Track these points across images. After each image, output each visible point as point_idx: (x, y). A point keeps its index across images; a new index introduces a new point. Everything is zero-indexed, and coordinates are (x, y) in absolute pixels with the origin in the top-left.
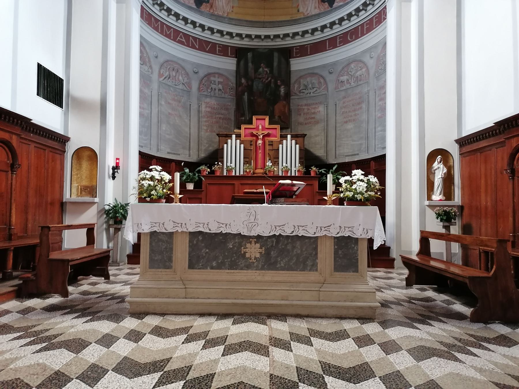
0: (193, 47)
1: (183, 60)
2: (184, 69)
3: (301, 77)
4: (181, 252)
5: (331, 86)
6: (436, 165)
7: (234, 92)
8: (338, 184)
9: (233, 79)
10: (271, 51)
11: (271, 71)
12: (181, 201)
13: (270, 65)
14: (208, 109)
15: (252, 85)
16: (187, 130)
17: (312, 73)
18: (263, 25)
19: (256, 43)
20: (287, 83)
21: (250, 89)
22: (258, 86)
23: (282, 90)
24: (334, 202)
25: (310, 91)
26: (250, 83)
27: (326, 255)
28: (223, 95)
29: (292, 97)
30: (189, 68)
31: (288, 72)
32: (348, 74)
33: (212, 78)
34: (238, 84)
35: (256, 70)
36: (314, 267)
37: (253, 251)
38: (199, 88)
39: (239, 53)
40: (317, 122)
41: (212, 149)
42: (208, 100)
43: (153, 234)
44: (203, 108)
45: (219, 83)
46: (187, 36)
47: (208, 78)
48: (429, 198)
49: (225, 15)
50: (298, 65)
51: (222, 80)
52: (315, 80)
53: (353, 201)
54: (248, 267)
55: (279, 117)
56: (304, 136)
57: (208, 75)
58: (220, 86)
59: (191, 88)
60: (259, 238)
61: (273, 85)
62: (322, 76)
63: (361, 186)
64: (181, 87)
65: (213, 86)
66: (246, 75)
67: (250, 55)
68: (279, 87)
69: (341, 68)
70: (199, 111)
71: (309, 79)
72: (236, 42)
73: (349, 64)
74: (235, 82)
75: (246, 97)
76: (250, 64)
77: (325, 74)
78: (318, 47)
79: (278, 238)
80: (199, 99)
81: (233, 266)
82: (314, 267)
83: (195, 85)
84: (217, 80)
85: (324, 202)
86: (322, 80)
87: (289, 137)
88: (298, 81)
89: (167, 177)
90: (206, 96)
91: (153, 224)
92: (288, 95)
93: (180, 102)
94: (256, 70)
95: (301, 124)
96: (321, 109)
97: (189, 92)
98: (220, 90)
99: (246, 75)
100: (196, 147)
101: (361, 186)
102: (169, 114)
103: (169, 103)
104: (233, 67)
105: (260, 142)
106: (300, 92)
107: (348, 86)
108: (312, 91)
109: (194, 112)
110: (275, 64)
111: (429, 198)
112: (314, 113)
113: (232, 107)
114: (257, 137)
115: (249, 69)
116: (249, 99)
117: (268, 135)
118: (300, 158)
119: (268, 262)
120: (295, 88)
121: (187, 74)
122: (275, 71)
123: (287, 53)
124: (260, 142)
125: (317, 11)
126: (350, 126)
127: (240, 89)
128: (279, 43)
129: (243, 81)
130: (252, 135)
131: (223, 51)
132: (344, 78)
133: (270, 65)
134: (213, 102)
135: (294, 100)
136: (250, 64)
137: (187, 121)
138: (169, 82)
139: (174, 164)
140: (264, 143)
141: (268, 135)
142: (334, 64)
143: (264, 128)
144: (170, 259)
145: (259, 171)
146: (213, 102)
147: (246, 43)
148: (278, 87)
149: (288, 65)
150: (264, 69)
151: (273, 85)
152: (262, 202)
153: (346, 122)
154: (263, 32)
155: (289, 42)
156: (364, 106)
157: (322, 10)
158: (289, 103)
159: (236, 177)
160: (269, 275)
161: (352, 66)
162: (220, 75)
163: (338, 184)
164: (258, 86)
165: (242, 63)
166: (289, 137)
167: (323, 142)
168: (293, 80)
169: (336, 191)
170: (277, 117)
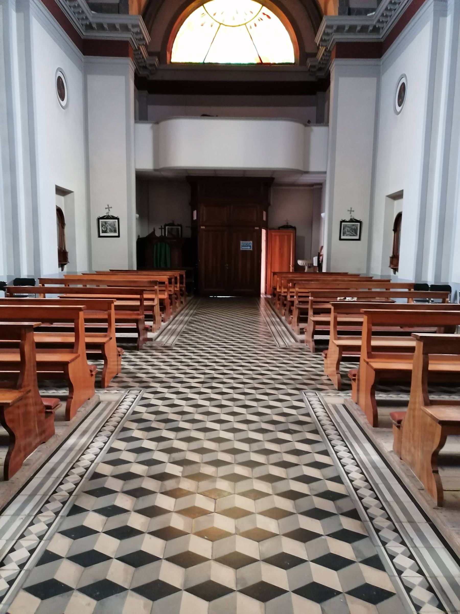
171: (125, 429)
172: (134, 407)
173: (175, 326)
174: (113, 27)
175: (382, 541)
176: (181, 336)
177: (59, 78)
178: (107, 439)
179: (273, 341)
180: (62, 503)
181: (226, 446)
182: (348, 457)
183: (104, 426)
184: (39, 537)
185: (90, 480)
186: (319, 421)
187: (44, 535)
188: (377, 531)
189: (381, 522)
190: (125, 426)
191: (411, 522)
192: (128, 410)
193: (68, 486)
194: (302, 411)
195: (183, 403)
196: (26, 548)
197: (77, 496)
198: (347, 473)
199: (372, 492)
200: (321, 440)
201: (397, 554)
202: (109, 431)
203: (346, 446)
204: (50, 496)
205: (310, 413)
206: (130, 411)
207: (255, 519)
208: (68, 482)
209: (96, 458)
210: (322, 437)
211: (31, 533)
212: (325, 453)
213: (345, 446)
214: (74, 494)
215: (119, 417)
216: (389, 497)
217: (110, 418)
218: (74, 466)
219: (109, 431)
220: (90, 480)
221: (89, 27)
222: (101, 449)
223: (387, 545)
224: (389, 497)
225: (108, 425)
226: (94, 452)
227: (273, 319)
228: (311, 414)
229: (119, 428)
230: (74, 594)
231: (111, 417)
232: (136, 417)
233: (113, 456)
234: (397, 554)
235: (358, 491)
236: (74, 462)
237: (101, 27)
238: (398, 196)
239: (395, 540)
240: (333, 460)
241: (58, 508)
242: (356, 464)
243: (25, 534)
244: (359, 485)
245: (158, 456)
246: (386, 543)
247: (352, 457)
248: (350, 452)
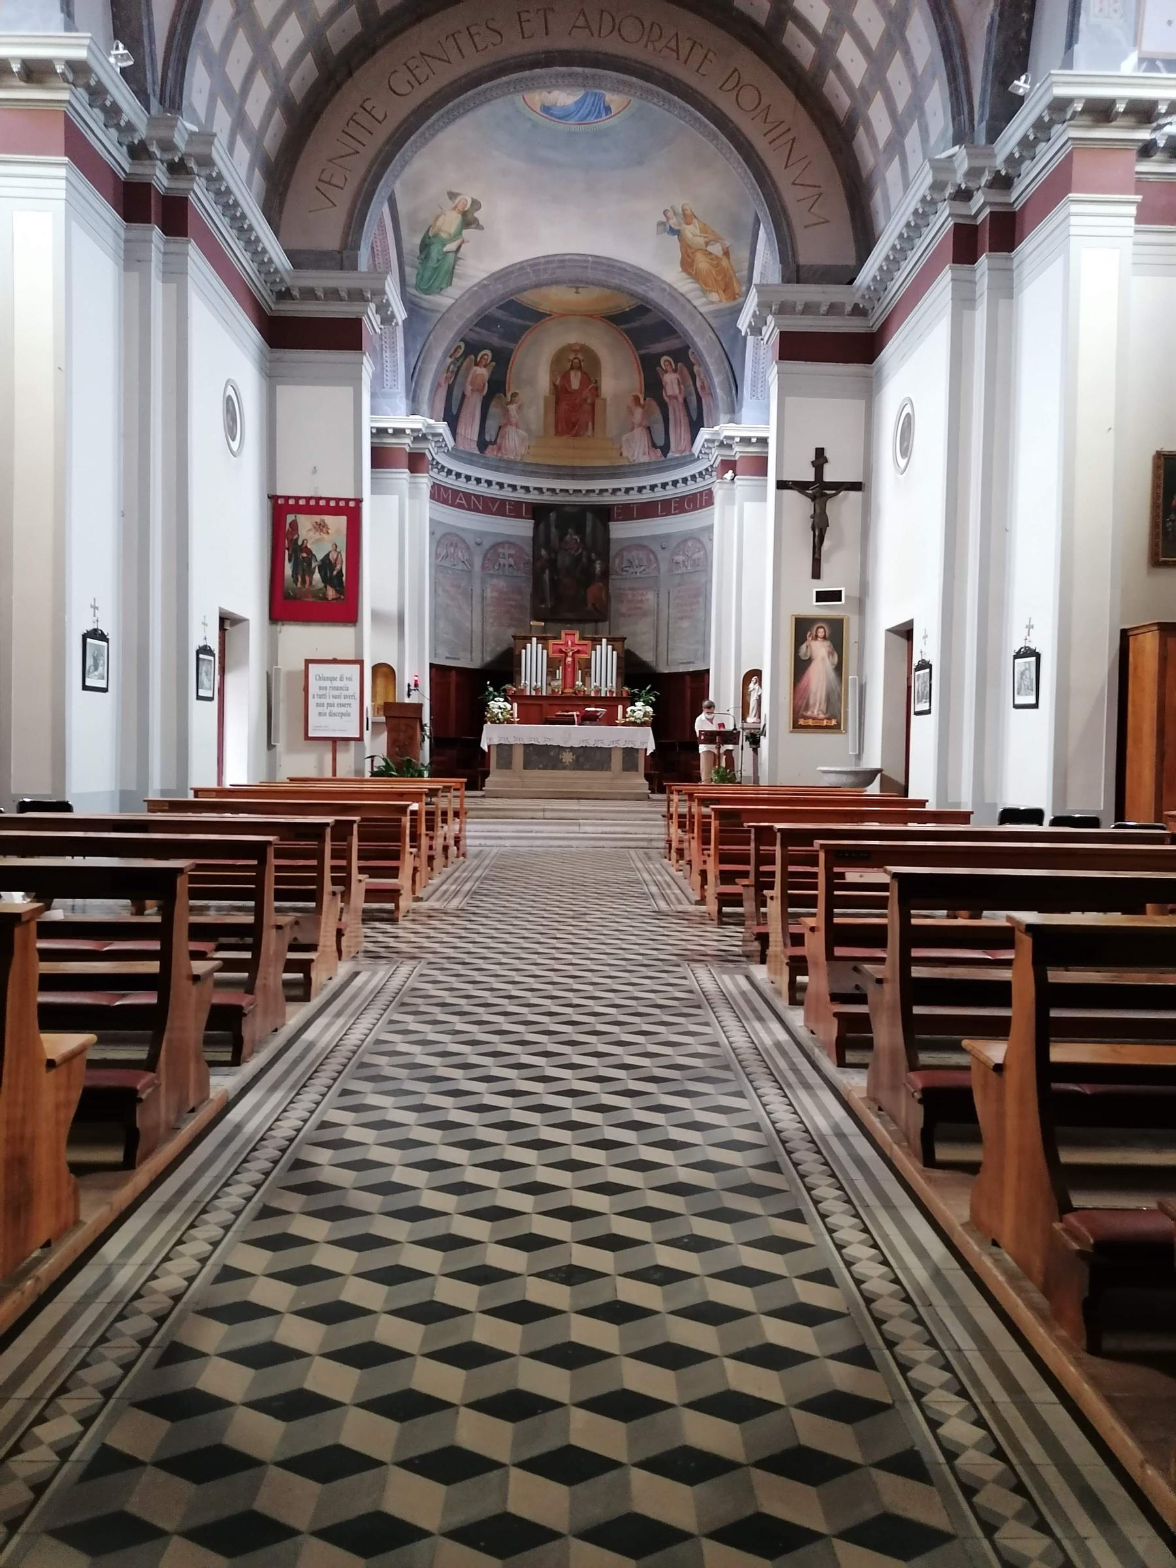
0: (476, 510)
1: (463, 529)
2: (464, 541)
3: (622, 550)
4: (518, 757)
5: (664, 567)
6: (751, 686)
7: (529, 568)
8: (625, 712)
9: (529, 549)
10: (585, 509)
11: (583, 539)
12: (518, 723)
13: (580, 530)
14: (495, 594)
15: (555, 560)
16: (468, 625)
17: (639, 545)
18: (573, 473)
19: (560, 499)
20: (605, 556)
21: (552, 564)
22: (564, 560)
23: (598, 567)
24: (623, 725)
25: (636, 569)
26: (553, 556)
27: (617, 760)
28: (515, 573)
29: (612, 577)
30: (470, 540)
31: (607, 541)
32: (684, 554)
33: (500, 550)
34: (536, 556)
35: (561, 538)
36: (609, 768)
37: (568, 757)
38: (483, 565)
39: (537, 512)
40: (645, 615)
41: (500, 649)
42: (495, 581)
43: (499, 746)
44: (489, 593)
45: (510, 556)
46: (467, 496)
47: (495, 549)
48: (744, 719)
49: (518, 459)
50: (620, 531)
51: (513, 552)
52: (642, 555)
53: (634, 724)
54: (564, 768)
55: (593, 605)
56: (623, 639)
57: (495, 546)
58: (511, 561)
59: (472, 565)
60: (572, 748)
61: (584, 560)
62: (653, 552)
63: (639, 714)
64: (460, 566)
65: (502, 561)
66: (547, 545)
67: (553, 515)
68: (594, 562)
69: (675, 544)
70: (483, 597)
71: (634, 553)
72: (534, 497)
73: (685, 541)
74: (531, 553)
75: (547, 576)
76: (553, 529)
77: (655, 547)
78: (648, 510)
79: (584, 749)
80: (483, 582)
81: (554, 768)
82: (609, 768)
83: (478, 562)
84: (507, 551)
85: (617, 725)
86: (652, 557)
87: (604, 641)
88: (620, 554)
89: (509, 706)
90: (492, 576)
91: (500, 738)
92: (606, 574)
93: (459, 587)
94: (561, 538)
95: (623, 615)
96: (650, 596)
97: (470, 572)
98: (510, 566)
99: (547, 545)
100: (480, 647)
101: (639, 714)
102: (448, 605)
103: (447, 591)
104: (529, 533)
105: (569, 659)
106: (622, 570)
107: (683, 570)
108: (639, 570)
109: (476, 599)
110: (588, 530)
111: (744, 719)
112: (641, 601)
113: (528, 589)
114: (566, 654)
115: (552, 536)
116: (551, 579)
117: (578, 652)
118: (618, 668)
119: (577, 765)
120: (615, 564)
121: (468, 547)
122: (588, 539)
123: (605, 514)
124: (569, 659)
125: (646, 459)
126: (685, 624)
127: (539, 564)
128: (594, 499)
129: (543, 552)
130: (561, 651)
131: (514, 509)
132: (680, 558)
133: (580, 530)
134: (502, 583)
135: (615, 583)
136: (553, 529)
137: (469, 612)
138: (447, 563)
139: (454, 673)
140: (574, 661)
141: (578, 652)
142: (668, 536)
143: (573, 644)
144: (511, 763)
145: (569, 691)
146: (502, 583)
147: (547, 498)
148: (591, 562)
149: (607, 530)
150: (572, 537)
151: (584, 560)
152: (573, 723)
153: (682, 618)
154: (571, 485)
155: (607, 499)
156: (701, 599)
157: (654, 459)
158: (607, 585)
159: (542, 697)
160: (580, 773)
161: (690, 544)
162: (511, 544)
163: (625, 712)
164: (564, 560)
165: (542, 526)
166: (604, 641)
167: (653, 643)
168: (612, 553)
169: (624, 717)
170: (590, 605)
171: (267, 1212)
172: (324, 1112)
173: (454, 887)
174: (333, 294)
175: (899, 1365)
176: (403, 1004)
177: (229, 399)
178: (198, 1265)
179: (685, 978)
180: (81, 1422)
181: (550, 1259)
182: (871, 1259)
183: (285, 1111)
184: (102, 1392)
185: (213, 1283)
186: (784, 1142)
187: (76, 1444)
188: (918, 1395)
189: (998, 1500)
190: (302, 1157)
191: (889, 1205)
192: (305, 1121)
193: (106, 1370)
194: (806, 1261)
195: (447, 1102)
196: (74, 1415)
197: (299, 1145)
198: (849, 1264)
199: (833, 1180)
200: (784, 1187)
201: (948, 1417)
202: (205, 1240)
203: (857, 1215)
204: (158, 1266)
205: (779, 1160)
206: (313, 1121)
207: (626, 1485)
208: (103, 1359)
209: (213, 1251)
210: (817, 1235)
211: (83, 1384)
212: (796, 1216)
213: (871, 1247)
214: (117, 1394)
215: (258, 1171)
216: (1035, 1451)
217: (232, 1175)
218: (184, 1239)
219: (205, 1240)
220: (213, 1283)
221: (284, 295)
222: (275, 1162)
223: (997, 1536)
224: (1035, 1451)
225: (239, 1182)
226: (184, 1269)
227: (659, 878)
228: (782, 1165)
229: (214, 1265)
230: (170, 1549)
231: (236, 1172)
232: (329, 1135)
233: (270, 1227)
234: (948, 1417)
235: (885, 1327)
236: (207, 1199)
237: (309, 294)
238: (906, 632)
239: (1020, 1516)
240: (817, 1235)
241: (70, 1437)
242: (862, 1227)
243: (68, 1385)
244: (878, 1290)
245: (357, 1292)
246: (996, 1529)
247: (893, 1277)
248: (866, 1230)
